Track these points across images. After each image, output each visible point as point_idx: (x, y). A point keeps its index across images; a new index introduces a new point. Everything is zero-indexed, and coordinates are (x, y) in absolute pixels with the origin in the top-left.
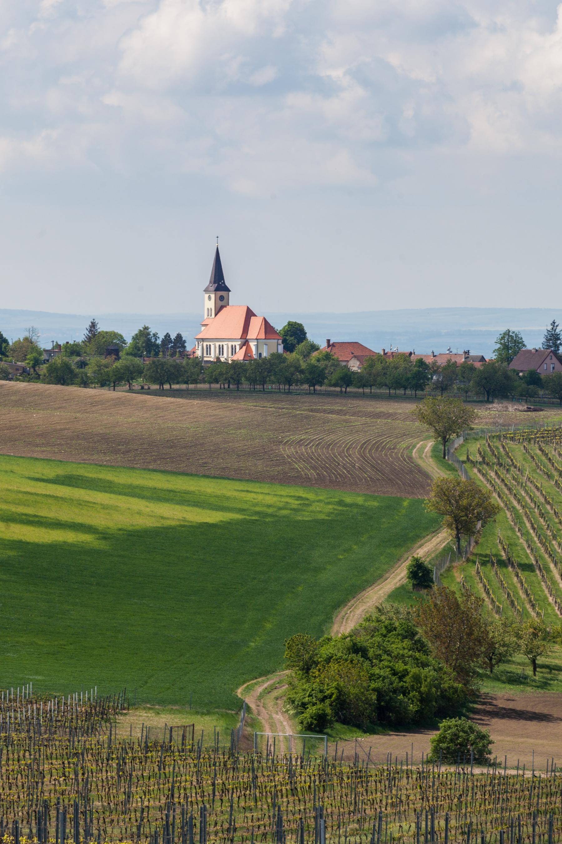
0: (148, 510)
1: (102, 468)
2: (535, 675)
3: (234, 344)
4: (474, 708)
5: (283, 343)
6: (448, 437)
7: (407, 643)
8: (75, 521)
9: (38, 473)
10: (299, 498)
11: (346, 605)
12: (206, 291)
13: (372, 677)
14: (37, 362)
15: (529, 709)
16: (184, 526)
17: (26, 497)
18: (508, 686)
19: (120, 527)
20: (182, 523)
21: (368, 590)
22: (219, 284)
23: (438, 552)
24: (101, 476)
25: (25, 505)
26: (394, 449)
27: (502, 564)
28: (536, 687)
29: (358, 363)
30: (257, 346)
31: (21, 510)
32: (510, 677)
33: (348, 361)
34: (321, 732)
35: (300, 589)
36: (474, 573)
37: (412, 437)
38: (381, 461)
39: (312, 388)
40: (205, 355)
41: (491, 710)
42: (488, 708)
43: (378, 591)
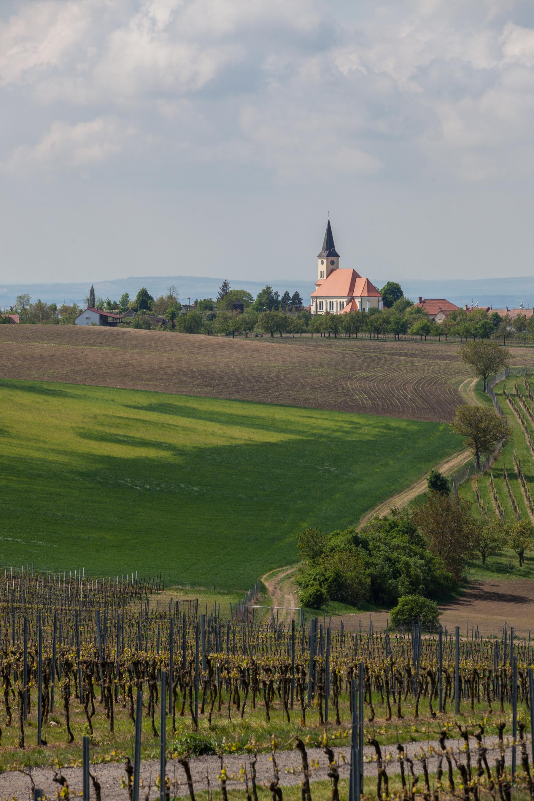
0: (221, 431)
1: (190, 398)
2: (521, 565)
3: (342, 300)
4: (463, 592)
5: (383, 300)
6: (487, 374)
7: (406, 537)
8: (158, 441)
9: (135, 402)
10: (352, 423)
11: (374, 509)
12: (320, 256)
13: (368, 565)
14: (173, 316)
15: (509, 593)
16: (250, 445)
17: (119, 421)
18: (496, 575)
19: (196, 445)
20: (248, 442)
21: (395, 497)
22: (330, 250)
23: (461, 466)
24: (188, 405)
25: (117, 427)
26: (444, 384)
27: (512, 476)
28: (519, 575)
29: (444, 317)
30: (361, 303)
31: (114, 431)
32: (500, 567)
33: (436, 315)
34: (318, 608)
35: (338, 495)
36: (488, 484)
37: (463, 374)
38: (430, 394)
39: (397, 336)
40: (318, 310)
41: (477, 593)
42: (476, 592)
43: (404, 498)
